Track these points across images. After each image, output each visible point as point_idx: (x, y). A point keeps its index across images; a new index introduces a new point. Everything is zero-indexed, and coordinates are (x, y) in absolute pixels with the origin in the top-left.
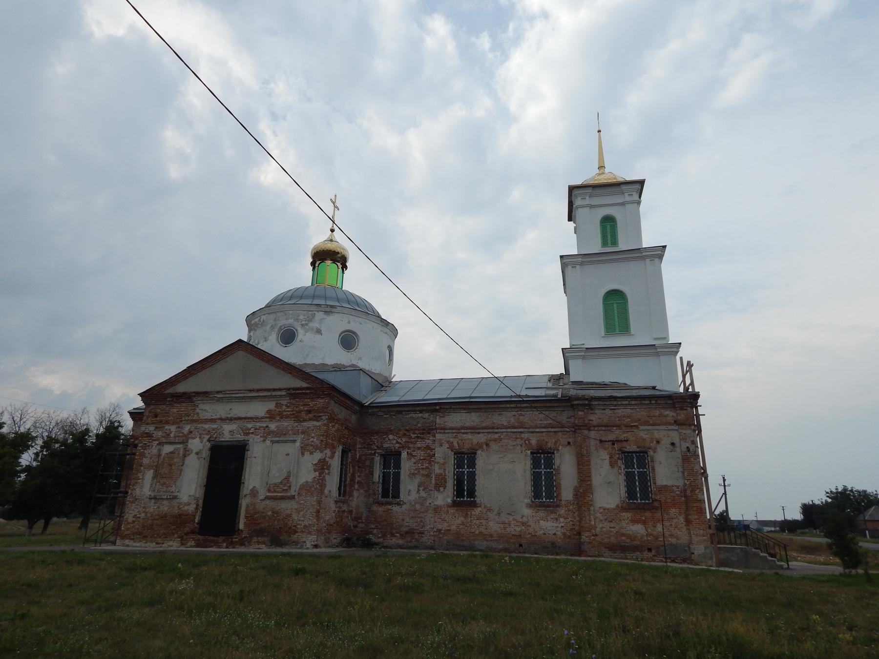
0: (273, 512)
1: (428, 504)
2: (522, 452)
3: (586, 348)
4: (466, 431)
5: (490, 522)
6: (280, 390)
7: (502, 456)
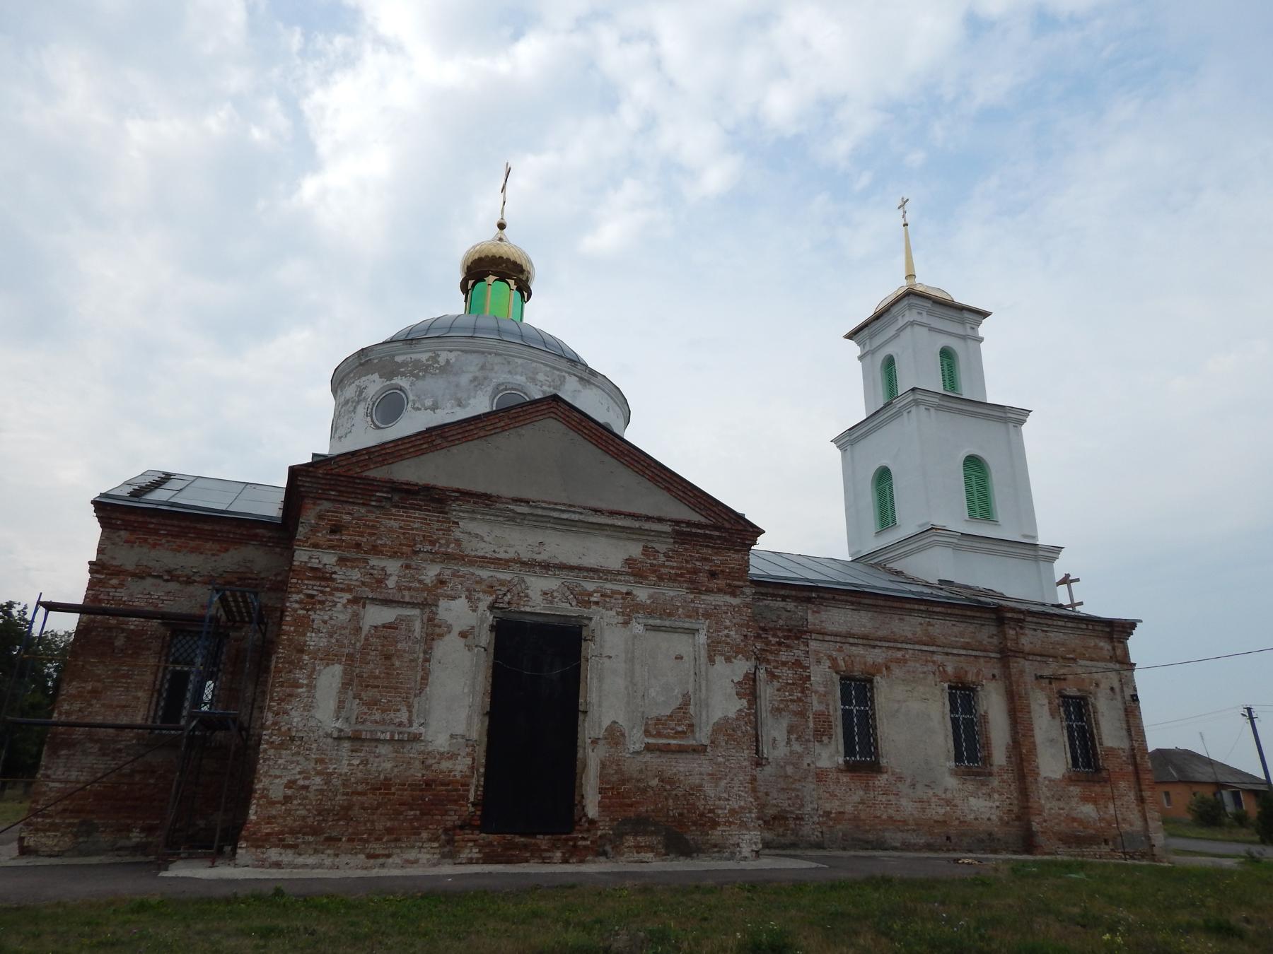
0: (662, 780)
1: (805, 765)
2: (936, 685)
3: (962, 534)
4: (856, 641)
5: (901, 799)
6: (660, 520)
7: (909, 688)
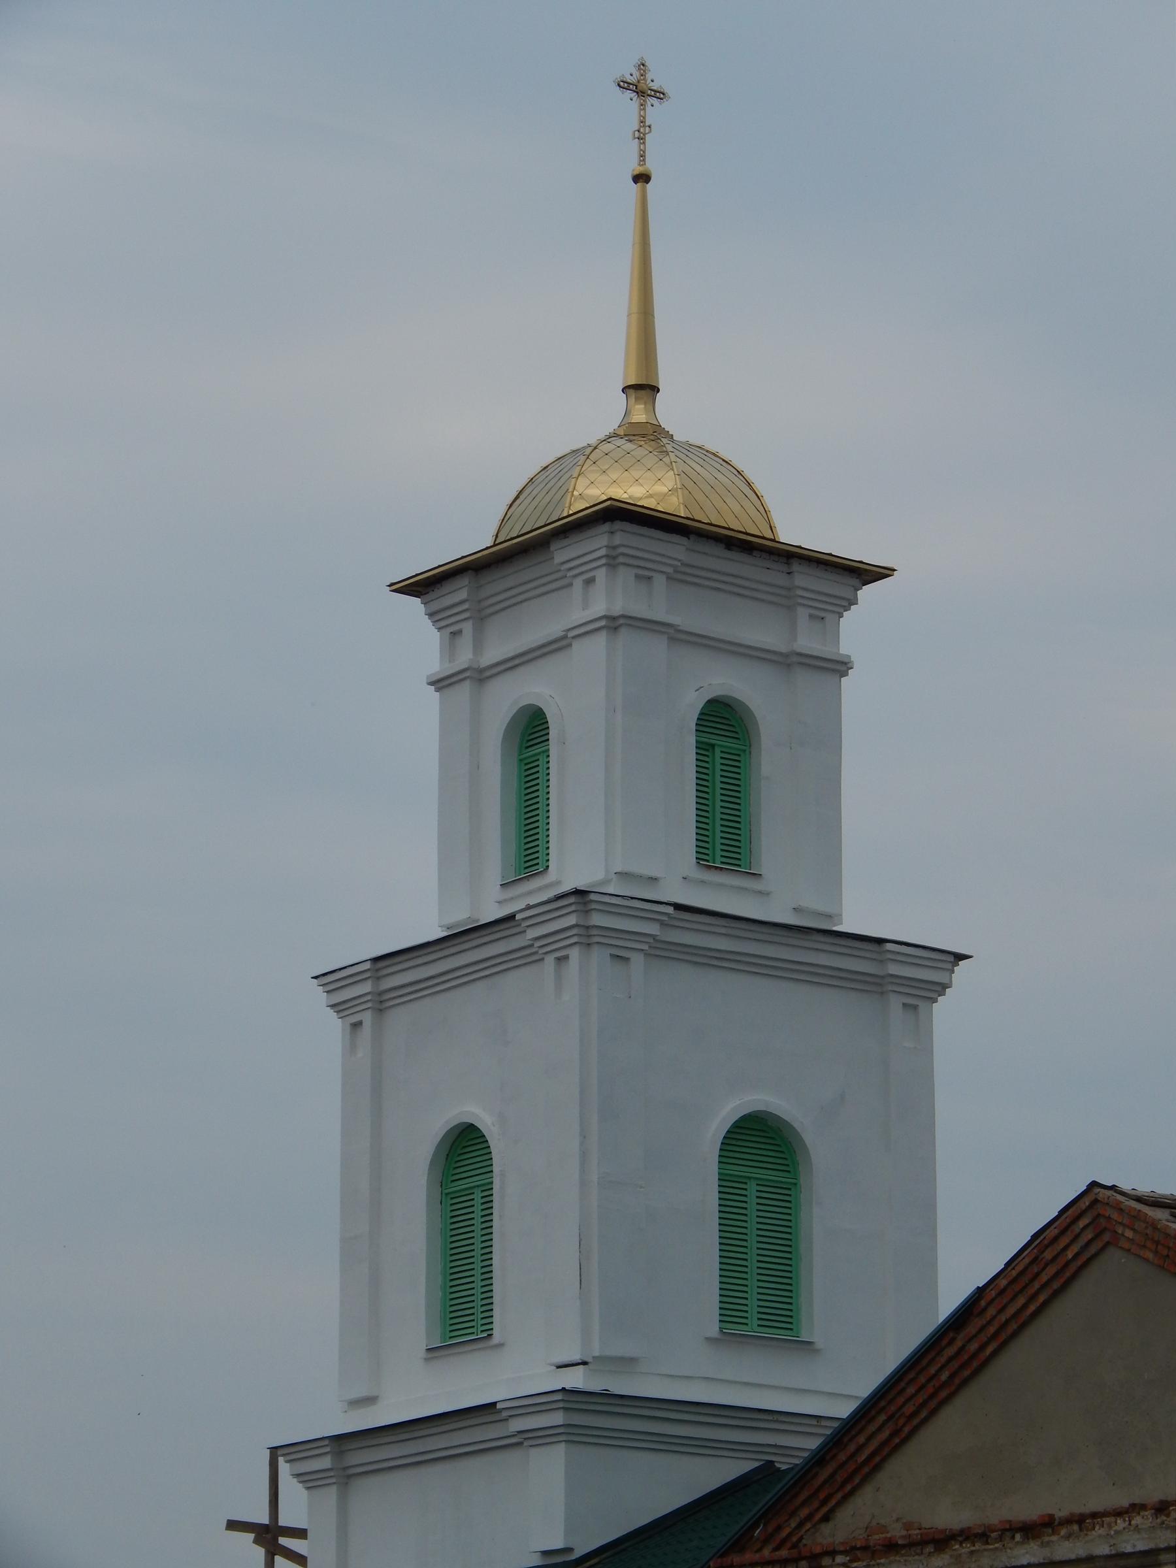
3: (678, 907)
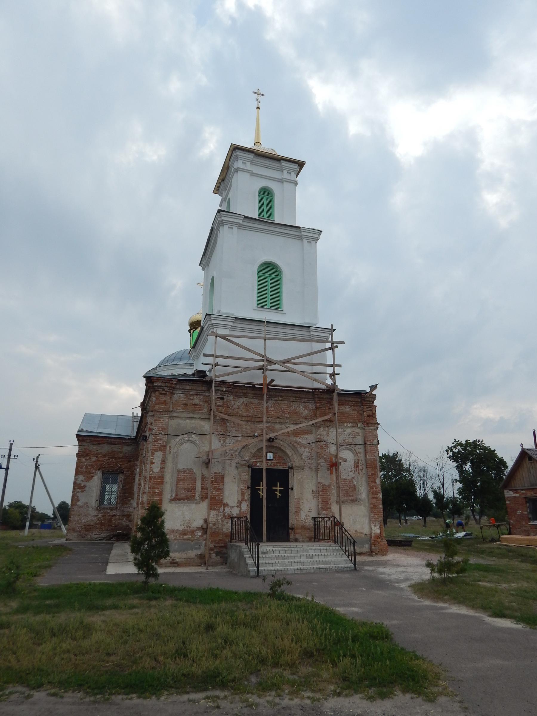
3: (236, 318)
